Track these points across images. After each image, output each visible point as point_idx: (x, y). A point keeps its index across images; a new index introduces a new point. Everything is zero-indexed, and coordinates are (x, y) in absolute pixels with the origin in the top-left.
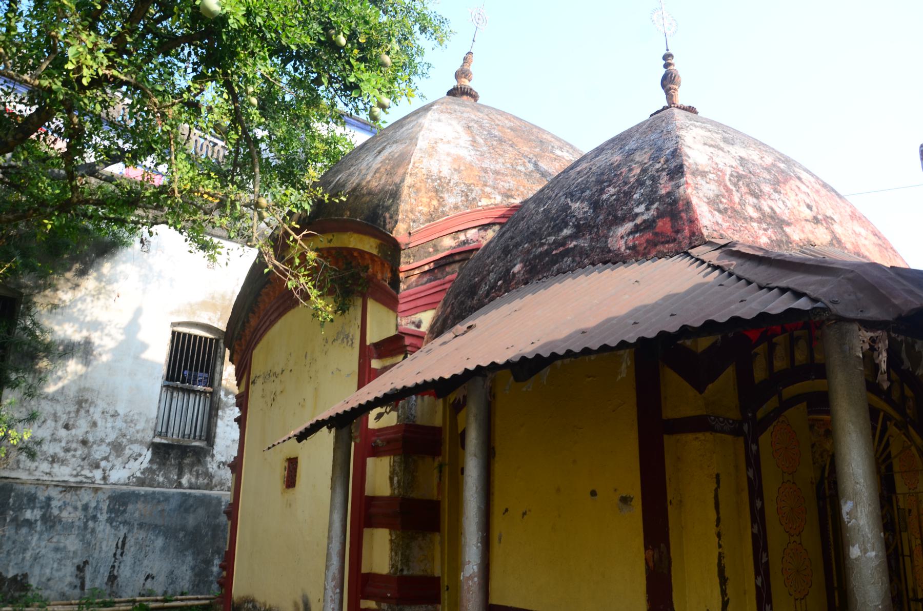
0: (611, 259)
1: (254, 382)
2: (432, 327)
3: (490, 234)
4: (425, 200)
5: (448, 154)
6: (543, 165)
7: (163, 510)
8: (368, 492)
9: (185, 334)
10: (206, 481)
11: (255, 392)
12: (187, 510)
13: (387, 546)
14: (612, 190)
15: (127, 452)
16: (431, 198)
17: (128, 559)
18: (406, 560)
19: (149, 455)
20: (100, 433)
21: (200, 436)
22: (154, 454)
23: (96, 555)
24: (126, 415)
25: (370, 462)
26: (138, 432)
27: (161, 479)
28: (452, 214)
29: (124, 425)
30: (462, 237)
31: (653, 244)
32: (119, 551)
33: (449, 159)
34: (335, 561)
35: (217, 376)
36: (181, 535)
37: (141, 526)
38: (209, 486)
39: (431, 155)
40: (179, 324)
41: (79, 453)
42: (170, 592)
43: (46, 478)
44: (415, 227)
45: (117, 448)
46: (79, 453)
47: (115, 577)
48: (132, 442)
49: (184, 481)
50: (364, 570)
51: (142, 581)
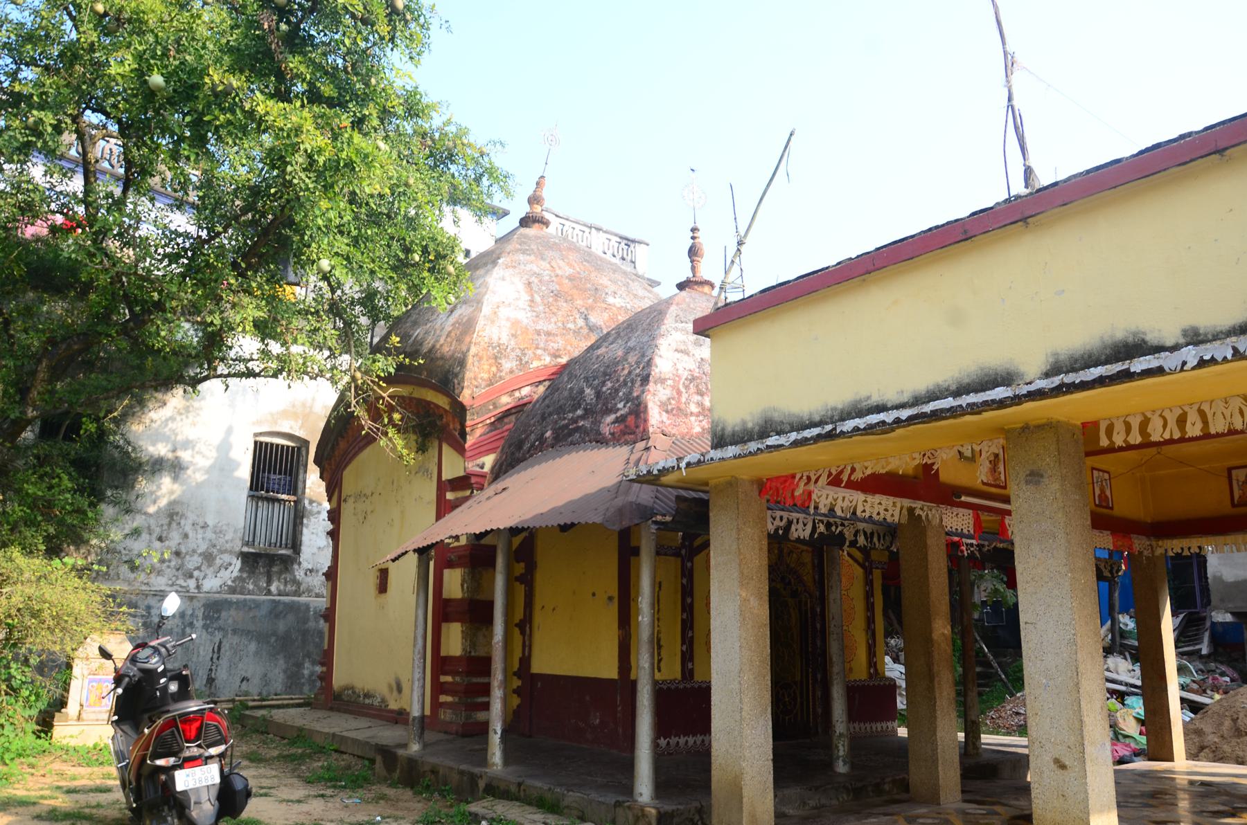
0: (601, 441)
2: (493, 468)
3: (541, 389)
4: (486, 367)
5: (508, 319)
6: (593, 319)
7: (254, 617)
8: (445, 595)
9: (267, 444)
12: (277, 616)
13: (460, 635)
14: (609, 384)
15: (218, 562)
16: (491, 365)
17: (224, 662)
18: (473, 645)
20: (191, 544)
22: (243, 563)
23: (194, 659)
24: (215, 527)
25: (446, 572)
27: (251, 587)
28: (508, 378)
30: (517, 394)
31: (623, 433)
32: (215, 656)
33: (508, 324)
34: (420, 641)
35: (300, 485)
36: (273, 639)
37: (235, 631)
38: (297, 593)
40: (261, 434)
41: (173, 564)
42: (264, 693)
43: (144, 588)
44: (478, 392)
45: (208, 558)
46: (173, 564)
47: (213, 680)
48: (222, 552)
49: (273, 588)
50: (443, 653)
51: (238, 683)
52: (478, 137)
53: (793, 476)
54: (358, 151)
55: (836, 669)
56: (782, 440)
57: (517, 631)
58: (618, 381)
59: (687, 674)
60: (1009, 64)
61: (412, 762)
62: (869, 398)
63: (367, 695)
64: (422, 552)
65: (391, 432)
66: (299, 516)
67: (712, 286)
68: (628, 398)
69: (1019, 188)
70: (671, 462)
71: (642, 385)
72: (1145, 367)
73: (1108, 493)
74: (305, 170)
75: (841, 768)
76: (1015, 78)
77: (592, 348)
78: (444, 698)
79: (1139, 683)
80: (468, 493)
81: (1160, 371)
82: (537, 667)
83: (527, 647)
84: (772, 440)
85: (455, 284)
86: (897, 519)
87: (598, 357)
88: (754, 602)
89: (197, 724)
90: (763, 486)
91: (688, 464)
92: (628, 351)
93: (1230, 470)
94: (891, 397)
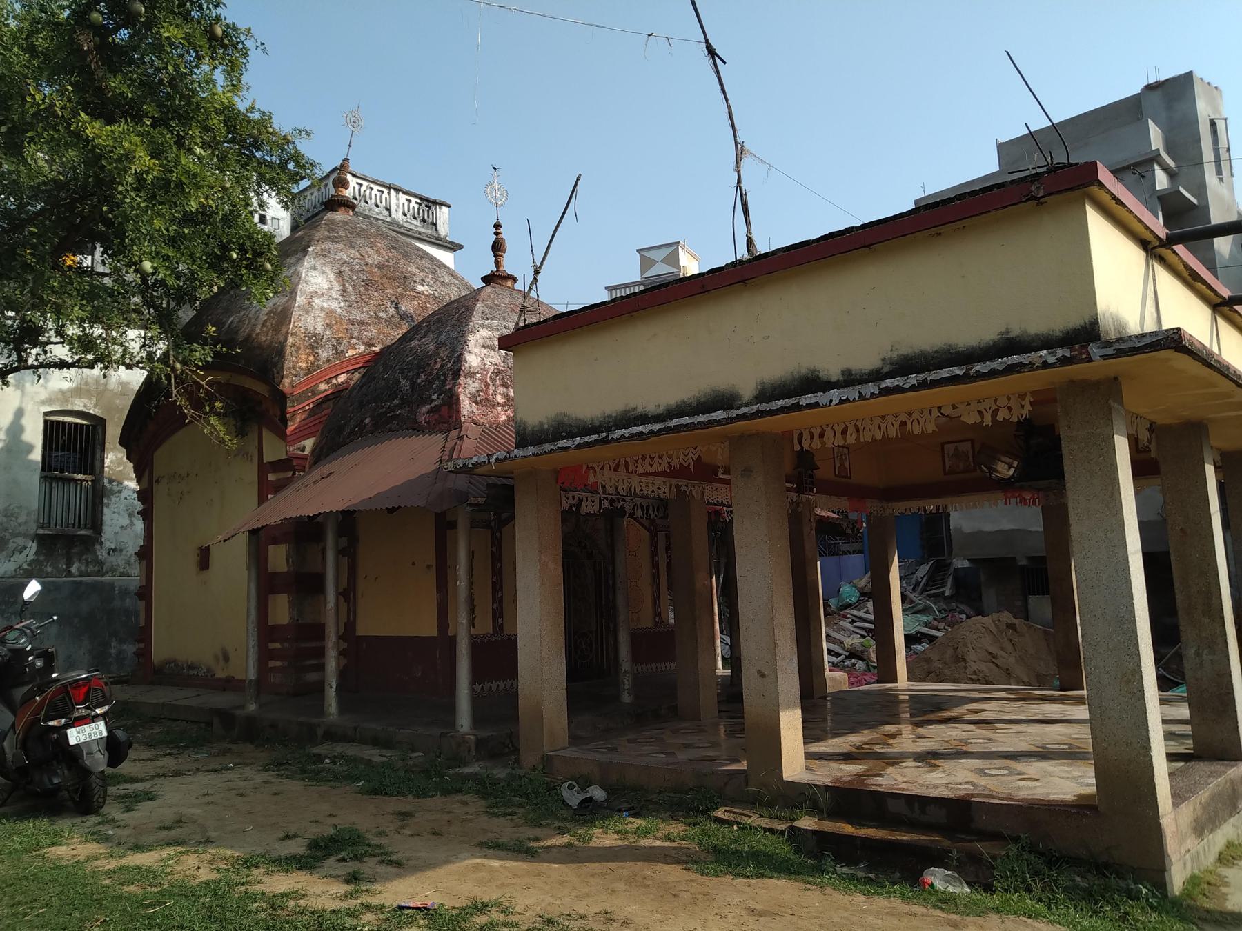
0: (418, 429)
1: (157, 481)
2: (313, 451)
3: (357, 376)
4: (304, 357)
5: (322, 309)
6: (404, 307)
10: (96, 568)
11: (160, 491)
14: (423, 377)
15: (11, 545)
16: (308, 355)
19: (34, 547)
22: (38, 546)
26: (20, 525)
27: (49, 569)
28: (325, 366)
29: (5, 519)
35: (98, 464)
36: (76, 620)
44: (297, 380)
49: (74, 570)
52: (282, 124)
53: (581, 466)
54: (186, 172)
55: (621, 618)
56: (569, 443)
57: (341, 598)
58: (431, 374)
59: (498, 628)
60: (740, 152)
63: (191, 667)
64: (254, 533)
65: (213, 420)
66: (99, 495)
67: (514, 280)
68: (441, 391)
69: (743, 253)
70: (483, 458)
72: (808, 402)
73: (847, 465)
74: (135, 189)
75: (626, 699)
77: (404, 339)
78: (272, 664)
79: (872, 617)
80: (290, 474)
81: (817, 405)
82: (361, 631)
83: (352, 612)
85: (272, 280)
86: (667, 495)
87: (411, 349)
88: (551, 566)
90: (557, 473)
91: (497, 460)
92: (440, 346)
93: (943, 445)
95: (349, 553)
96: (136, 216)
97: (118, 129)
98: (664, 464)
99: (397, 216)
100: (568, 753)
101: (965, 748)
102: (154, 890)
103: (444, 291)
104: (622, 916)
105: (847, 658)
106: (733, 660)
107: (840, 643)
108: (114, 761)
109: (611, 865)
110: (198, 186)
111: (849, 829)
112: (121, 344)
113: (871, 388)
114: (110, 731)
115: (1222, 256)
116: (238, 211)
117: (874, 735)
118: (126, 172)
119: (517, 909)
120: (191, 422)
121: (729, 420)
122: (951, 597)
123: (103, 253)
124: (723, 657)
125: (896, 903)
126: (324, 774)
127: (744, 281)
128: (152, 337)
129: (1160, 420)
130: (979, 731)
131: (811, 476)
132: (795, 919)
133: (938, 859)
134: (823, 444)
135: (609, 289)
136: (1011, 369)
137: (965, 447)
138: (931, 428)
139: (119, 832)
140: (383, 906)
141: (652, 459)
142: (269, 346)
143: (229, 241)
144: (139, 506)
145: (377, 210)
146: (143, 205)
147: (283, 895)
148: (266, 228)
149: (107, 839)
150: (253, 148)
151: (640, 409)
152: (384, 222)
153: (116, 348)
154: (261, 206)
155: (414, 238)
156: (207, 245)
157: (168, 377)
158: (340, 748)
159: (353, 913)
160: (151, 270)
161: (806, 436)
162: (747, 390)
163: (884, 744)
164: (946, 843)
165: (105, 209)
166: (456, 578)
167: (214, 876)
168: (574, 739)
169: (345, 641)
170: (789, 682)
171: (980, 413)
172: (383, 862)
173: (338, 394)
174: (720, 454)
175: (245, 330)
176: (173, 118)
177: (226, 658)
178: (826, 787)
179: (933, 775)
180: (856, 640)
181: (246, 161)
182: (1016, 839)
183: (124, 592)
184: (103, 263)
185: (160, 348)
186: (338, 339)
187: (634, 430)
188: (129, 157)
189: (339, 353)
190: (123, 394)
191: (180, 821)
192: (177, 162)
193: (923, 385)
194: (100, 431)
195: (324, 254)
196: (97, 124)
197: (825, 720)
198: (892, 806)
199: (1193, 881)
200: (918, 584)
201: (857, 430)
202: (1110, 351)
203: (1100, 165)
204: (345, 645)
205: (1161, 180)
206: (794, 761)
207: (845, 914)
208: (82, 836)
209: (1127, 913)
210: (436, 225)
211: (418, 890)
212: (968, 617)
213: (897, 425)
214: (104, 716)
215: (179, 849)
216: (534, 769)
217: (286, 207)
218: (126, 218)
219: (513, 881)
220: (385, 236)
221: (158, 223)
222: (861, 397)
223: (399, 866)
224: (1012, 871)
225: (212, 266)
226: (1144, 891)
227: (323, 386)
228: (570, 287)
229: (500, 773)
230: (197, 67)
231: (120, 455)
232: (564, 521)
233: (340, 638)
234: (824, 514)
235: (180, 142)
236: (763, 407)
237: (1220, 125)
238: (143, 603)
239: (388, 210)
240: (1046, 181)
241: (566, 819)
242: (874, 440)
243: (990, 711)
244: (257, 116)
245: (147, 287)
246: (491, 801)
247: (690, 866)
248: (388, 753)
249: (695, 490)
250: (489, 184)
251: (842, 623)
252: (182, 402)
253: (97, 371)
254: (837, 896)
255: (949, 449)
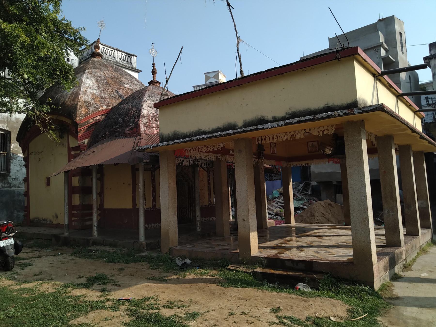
0: (125, 136)
1: (31, 154)
2: (88, 143)
3: (103, 117)
4: (84, 110)
5: (91, 93)
6: (120, 92)
11: (32, 157)
16: (86, 109)
21: (4, 170)
28: (92, 113)
33: (91, 95)
35: (8, 148)
38: (10, 187)
39: (85, 94)
44: (82, 118)
52: (75, 25)
53: (183, 149)
54: (40, 42)
56: (178, 141)
57: (98, 195)
60: (238, 40)
61: (66, 238)
62: (202, 129)
64: (66, 172)
65: (51, 132)
67: (160, 83)
68: (133, 122)
69: (239, 76)
70: (148, 146)
71: (138, 118)
74: (20, 48)
75: (199, 229)
76: (240, 44)
77: (120, 104)
78: (73, 219)
79: (283, 202)
81: (263, 128)
82: (106, 206)
84: (176, 141)
85: (72, 82)
87: (123, 108)
88: (172, 184)
89: (6, 227)
90: (174, 152)
91: (153, 147)
92: (133, 106)
93: (308, 142)
94: (207, 129)
95: (101, 179)
96: (21, 58)
97: (14, 25)
98: (212, 149)
99: (118, 59)
100: (178, 248)
101: (312, 245)
102: (33, 295)
103: (135, 87)
104: (196, 300)
105: (275, 215)
106: (235, 217)
107: (272, 210)
108: (17, 252)
109: (192, 284)
110: (44, 48)
111: (272, 271)
112: (16, 104)
113: (282, 123)
114: (15, 242)
115: (402, 79)
116: (59, 57)
117: (282, 241)
118: (17, 41)
119: (160, 299)
120: (43, 133)
121: (234, 133)
122: (310, 195)
123: (9, 71)
124: (232, 216)
125: (287, 295)
126: (93, 256)
127: (239, 85)
128: (28, 102)
129: (379, 134)
130: (317, 239)
131: (263, 153)
132: (253, 300)
133: (301, 280)
134: (266, 142)
135: (194, 87)
136: (328, 117)
137: (315, 143)
138: (302, 137)
139: (19, 276)
140: (114, 299)
141: (208, 147)
142: (71, 106)
143: (56, 68)
144: (24, 163)
145: (110, 57)
146: (23, 54)
147: (78, 296)
148: (69, 63)
149: (15, 279)
150: (64, 34)
151: (203, 129)
152: (113, 62)
153: (15, 106)
154: (67, 55)
155: (124, 68)
156: (48, 69)
157: (34, 116)
158: (98, 247)
159: (103, 302)
160: (27, 78)
161: (260, 139)
162: (240, 123)
163: (285, 244)
164: (304, 275)
165: (9, 55)
166: (139, 188)
167: (54, 291)
168: (180, 243)
169: (100, 210)
170: (253, 223)
171: (319, 132)
172: (113, 285)
173: (97, 123)
174: (231, 145)
175: (62, 100)
176: (34, 22)
177: (57, 217)
178: (265, 258)
179: (301, 253)
180: (278, 209)
181: (62, 37)
182: (327, 274)
183: (19, 194)
184: (9, 75)
185: (31, 106)
186: (96, 104)
187: (201, 137)
188: (18, 36)
189: (97, 109)
190: (17, 122)
191: (41, 273)
192: (36, 38)
193: (299, 122)
194: (9, 136)
195: (91, 73)
196: (5, 24)
197: (267, 236)
198: (287, 264)
199: (383, 286)
200: (299, 190)
201: (277, 138)
202: (360, 111)
203: (359, 49)
204: (100, 212)
205: (383, 53)
206: (255, 249)
207: (270, 299)
208: (6, 278)
209: (361, 296)
210: (132, 63)
211: (126, 294)
212: (316, 201)
213: (291, 136)
214: (13, 237)
215: (41, 282)
216: (166, 253)
217: (77, 56)
218: (17, 59)
219: (159, 290)
220: (113, 67)
221: (29, 61)
222: (278, 126)
223: (119, 286)
224: (325, 284)
225: (49, 77)
226: (367, 289)
227: (91, 121)
228: (179, 86)
229: (154, 255)
230: (43, 3)
231: (16, 145)
232: (177, 169)
233: (98, 209)
234: (267, 166)
235: (37, 31)
236: (245, 129)
237: (403, 34)
238: (26, 197)
239: (114, 57)
240: (342, 53)
241: (177, 270)
242: (283, 140)
243: (321, 232)
244: (65, 22)
245: (26, 84)
246: (151, 264)
247: (219, 284)
248: (115, 249)
249: (223, 158)
250: (151, 49)
251: (273, 204)
252: (39, 125)
253: (7, 114)
254: (268, 293)
255: (310, 144)
